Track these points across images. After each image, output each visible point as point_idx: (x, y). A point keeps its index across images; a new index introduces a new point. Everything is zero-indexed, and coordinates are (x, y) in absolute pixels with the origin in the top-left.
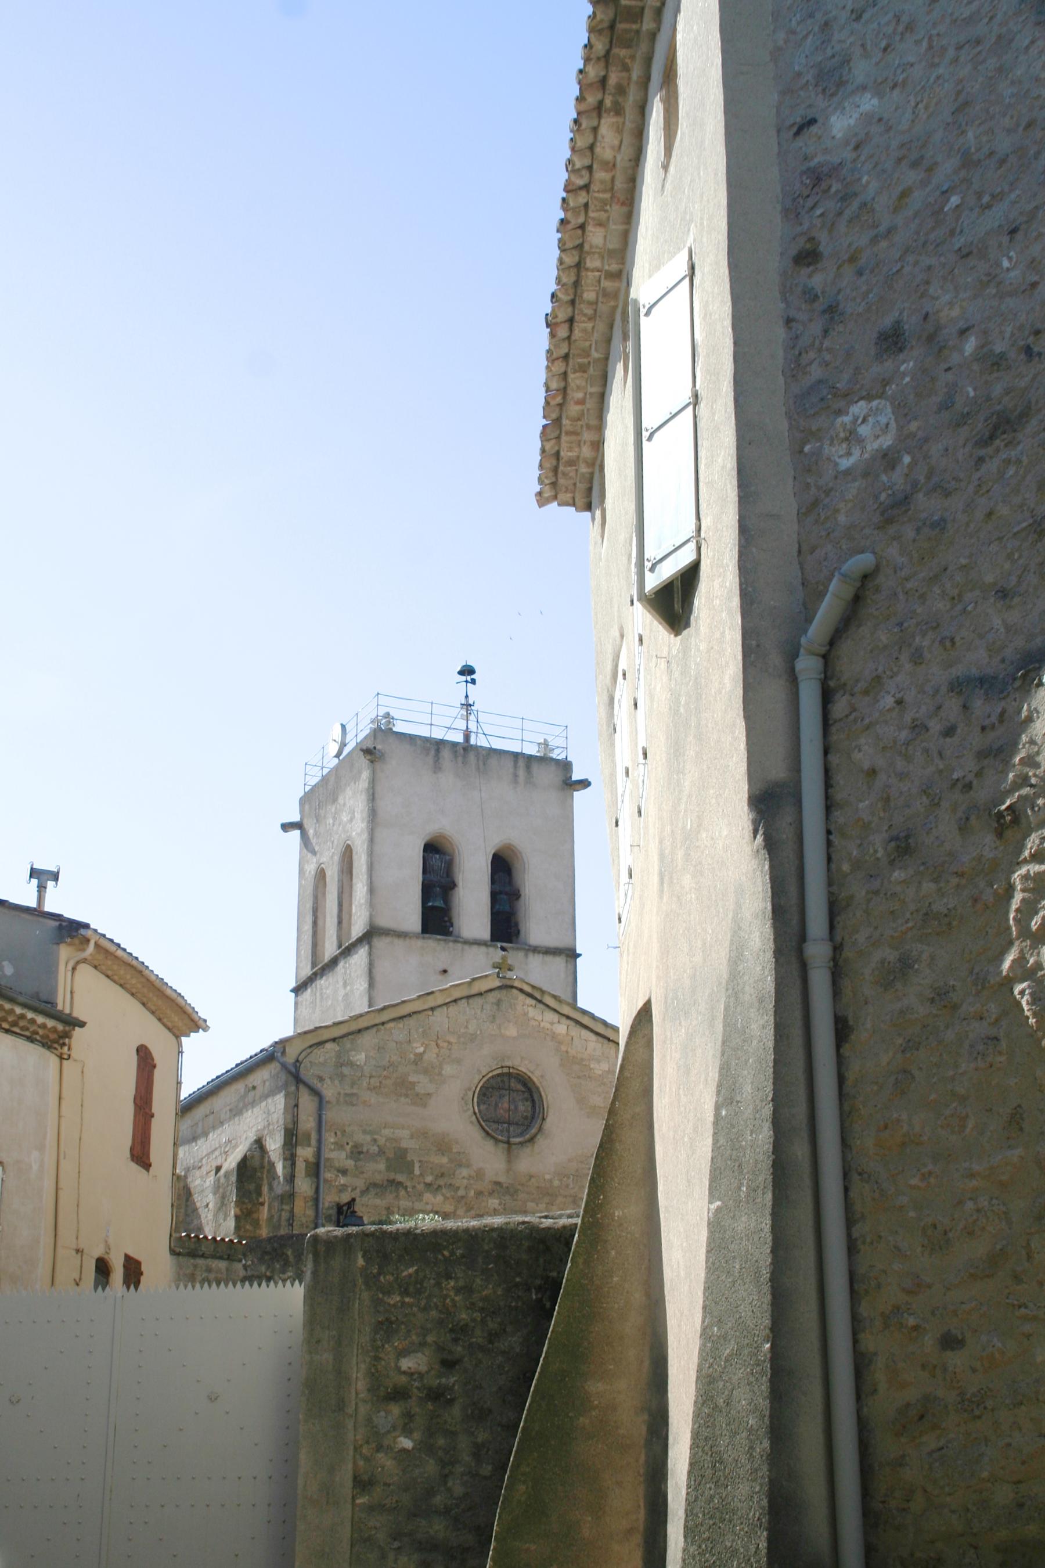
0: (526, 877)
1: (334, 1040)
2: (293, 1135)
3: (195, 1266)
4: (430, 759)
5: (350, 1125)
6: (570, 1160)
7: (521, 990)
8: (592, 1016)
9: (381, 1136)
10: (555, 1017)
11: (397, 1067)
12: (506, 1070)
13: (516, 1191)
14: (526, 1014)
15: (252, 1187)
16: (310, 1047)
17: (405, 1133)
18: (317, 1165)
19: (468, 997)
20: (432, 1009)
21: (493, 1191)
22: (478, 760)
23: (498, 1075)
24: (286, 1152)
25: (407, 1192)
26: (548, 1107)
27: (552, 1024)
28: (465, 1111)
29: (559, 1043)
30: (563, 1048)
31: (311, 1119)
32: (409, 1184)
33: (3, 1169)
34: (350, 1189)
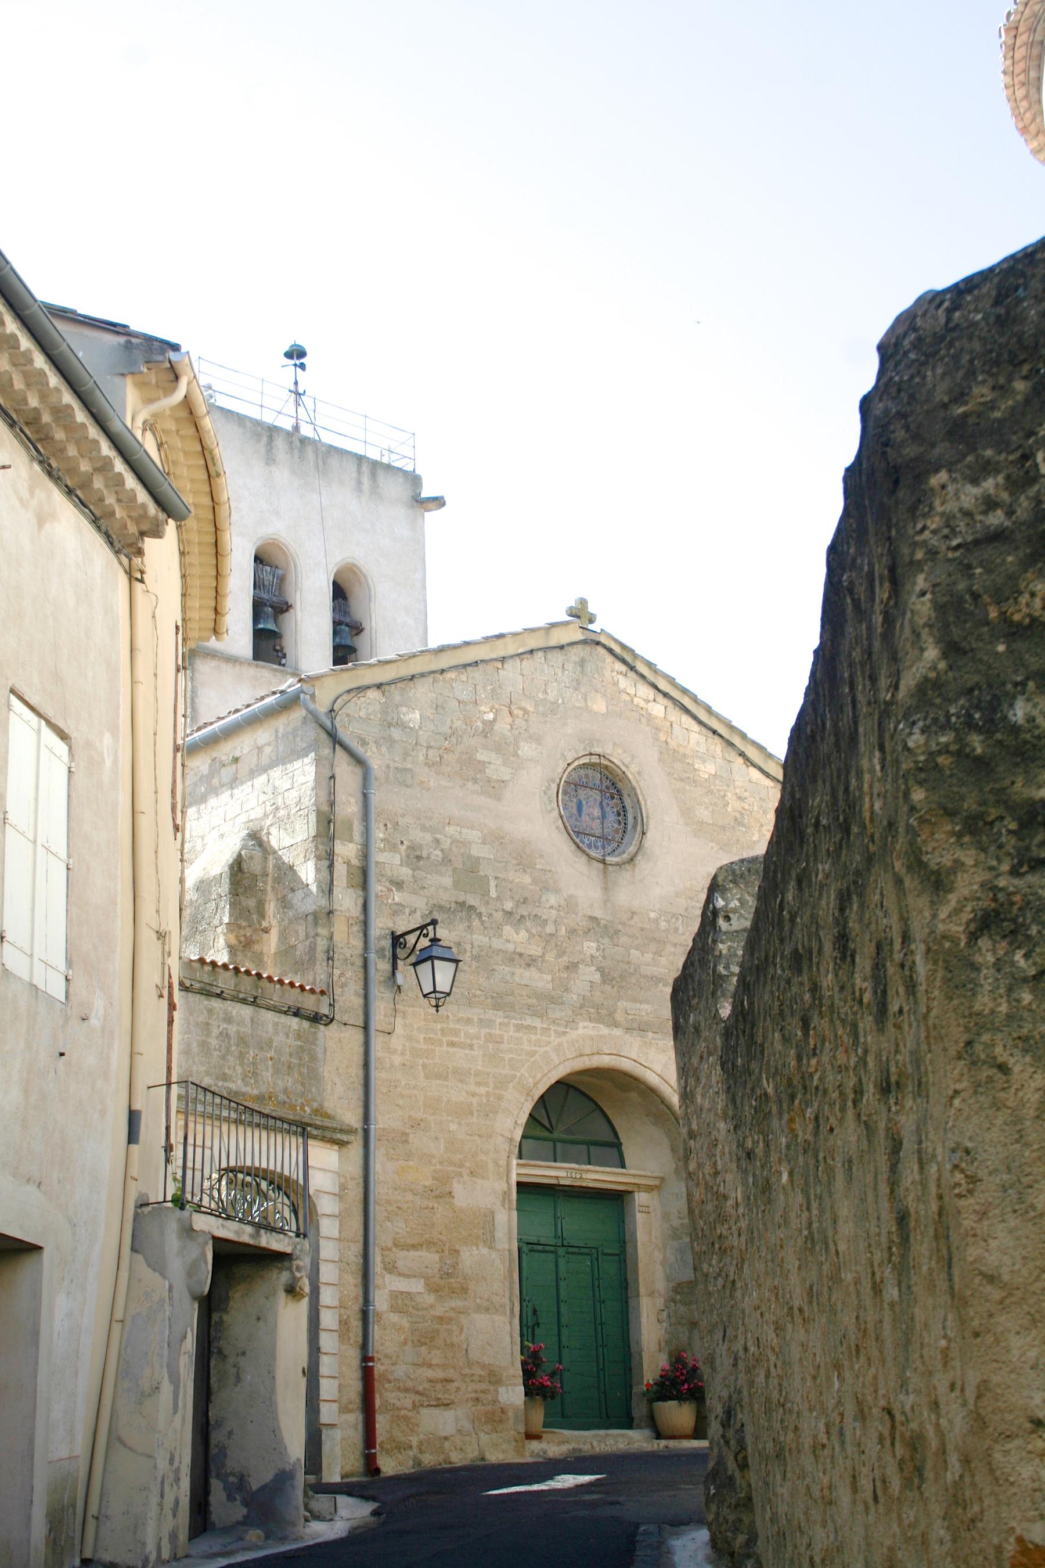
0: (372, 606)
1: (379, 686)
2: (329, 822)
3: (210, 1011)
4: (262, 446)
5: (403, 815)
6: (677, 895)
7: (610, 651)
8: (695, 699)
9: (445, 836)
10: (650, 693)
11: (461, 737)
12: (595, 759)
13: (617, 932)
14: (616, 684)
15: (252, 903)
16: (349, 691)
17: (474, 835)
18: (365, 872)
19: (546, 649)
20: (503, 660)
21: (589, 930)
22: (317, 455)
23: (584, 766)
24: (320, 847)
25: (483, 923)
26: (647, 817)
27: (647, 701)
28: (550, 811)
29: (657, 729)
30: (662, 737)
31: (352, 800)
32: (483, 910)
33: (70, 748)
34: (407, 911)
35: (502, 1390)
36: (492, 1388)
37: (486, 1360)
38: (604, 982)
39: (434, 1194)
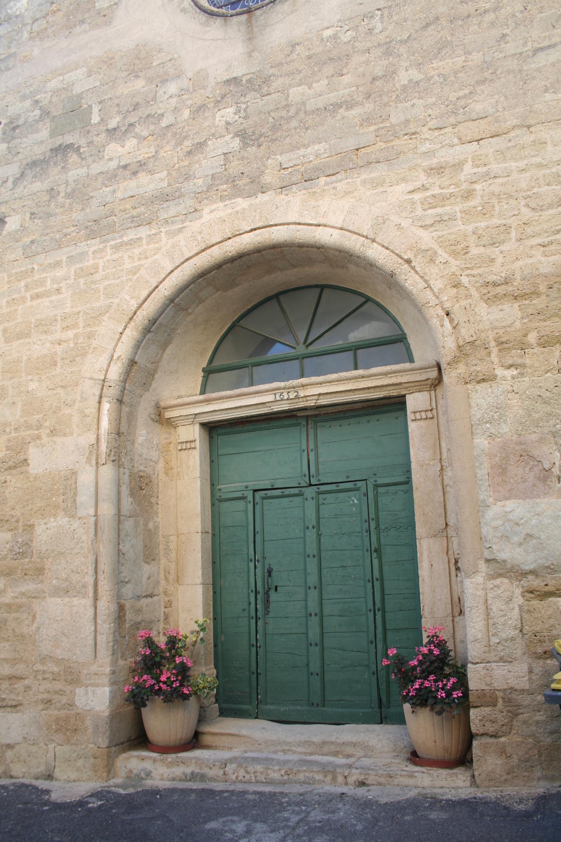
35: (79, 691)
36: (68, 688)
37: (59, 654)
38: (245, 144)
39: (6, 466)
